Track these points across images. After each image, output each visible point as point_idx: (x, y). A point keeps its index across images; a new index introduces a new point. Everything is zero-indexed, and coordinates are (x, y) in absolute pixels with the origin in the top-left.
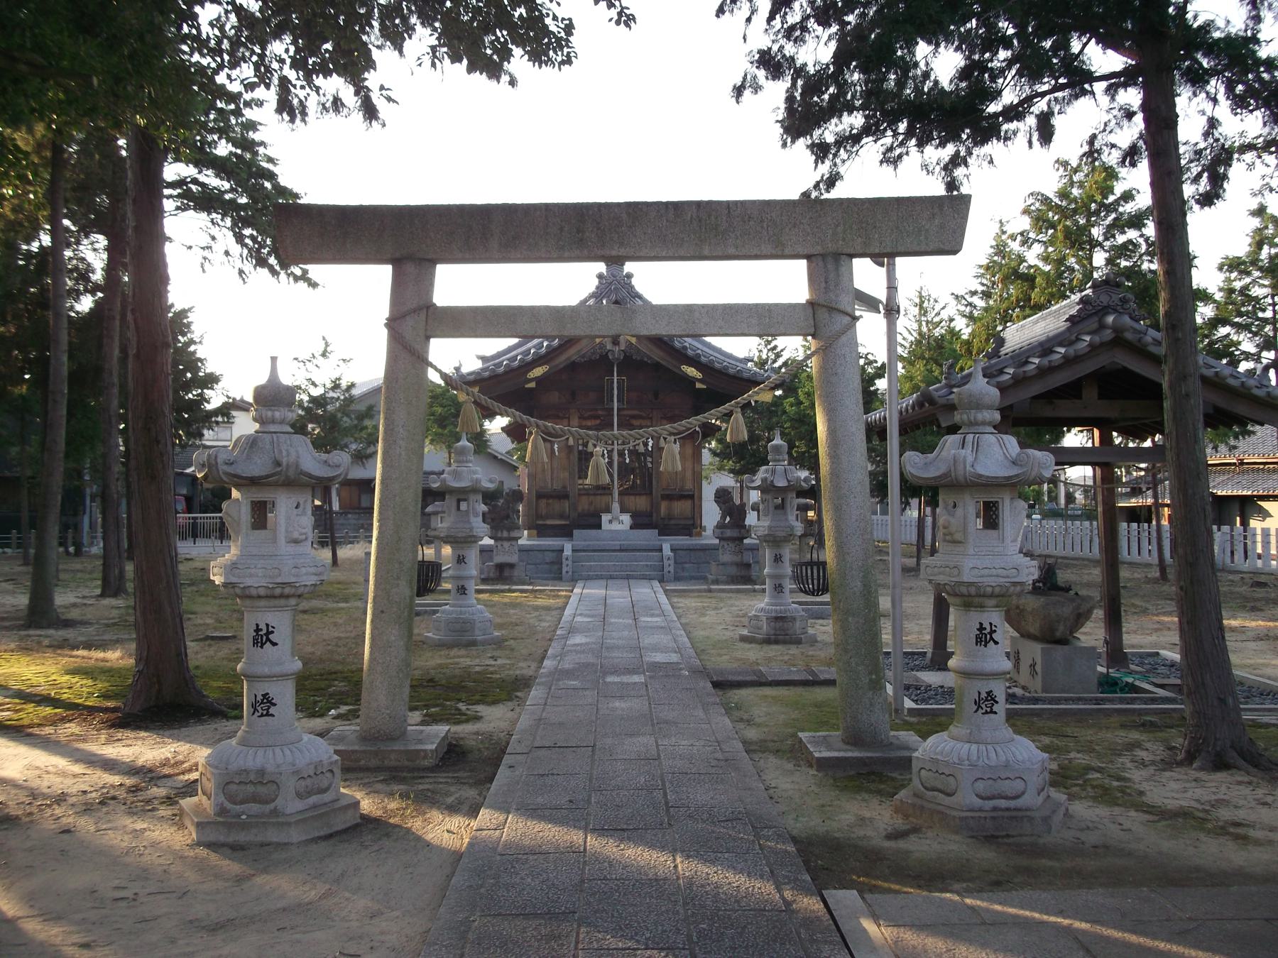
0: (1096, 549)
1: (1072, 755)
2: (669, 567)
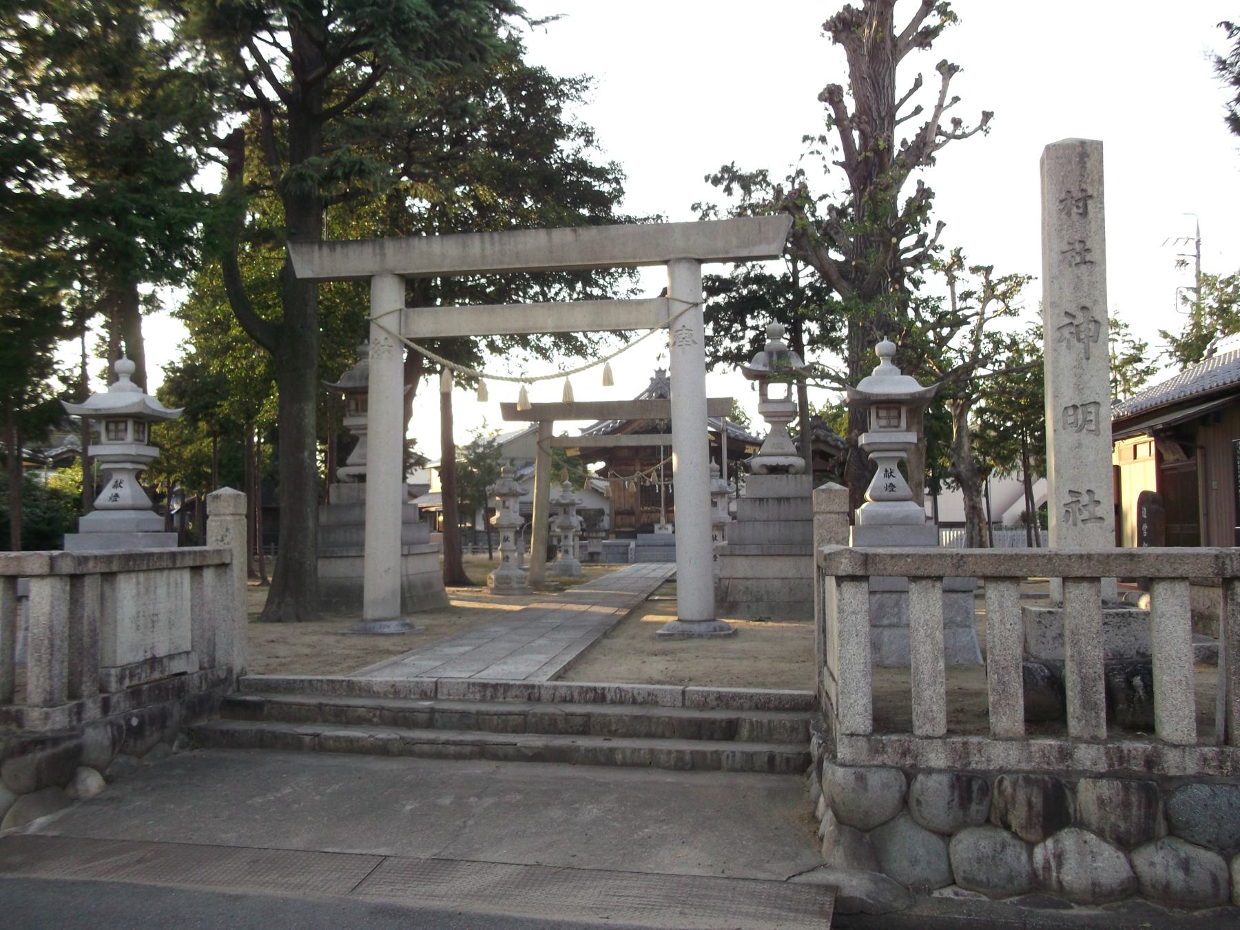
1: (152, 764)
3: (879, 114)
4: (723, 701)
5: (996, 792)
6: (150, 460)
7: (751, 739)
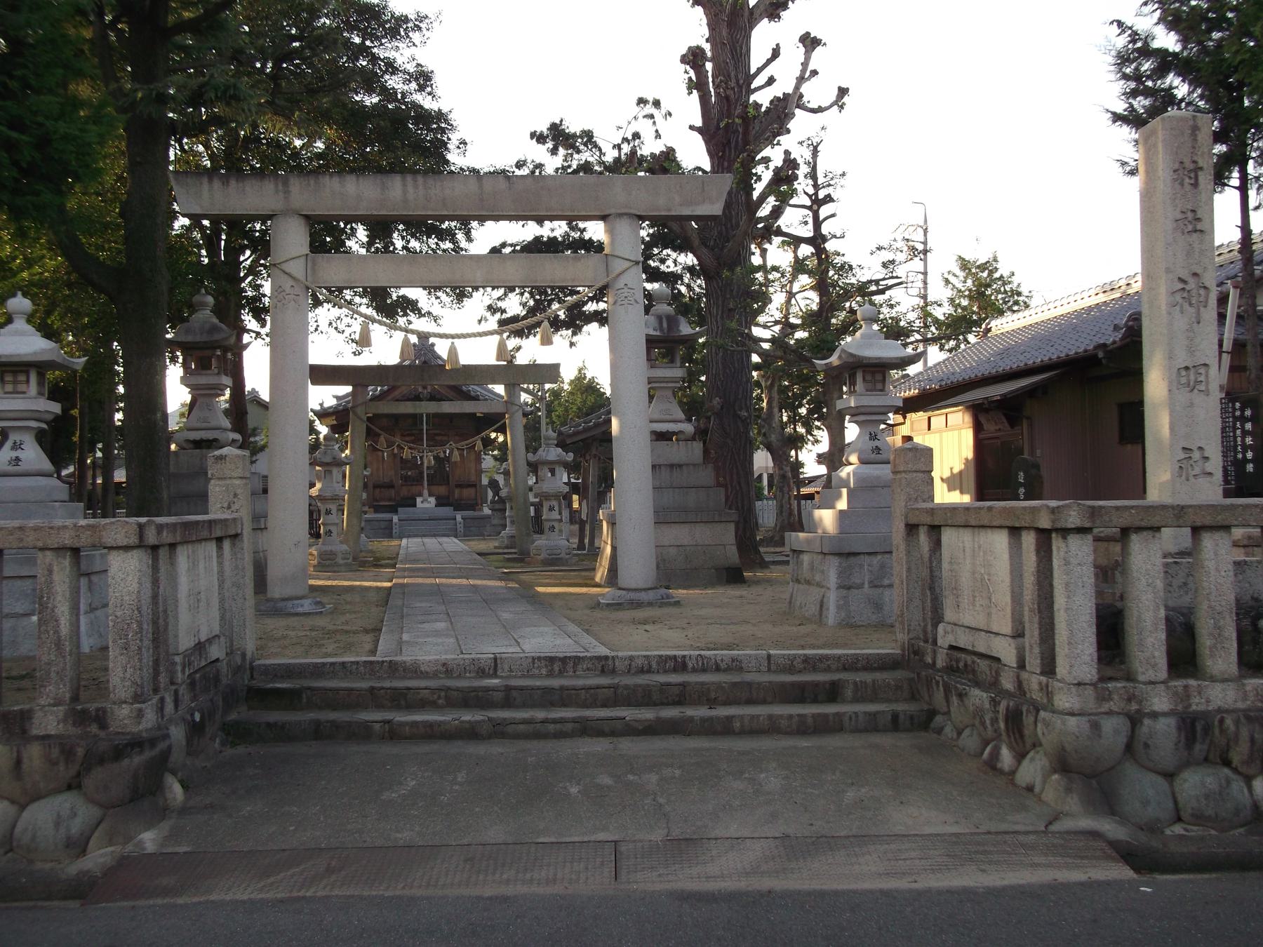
2: (460, 528)
3: (738, 81)
4: (811, 664)
5: (1217, 731)
6: (50, 417)
7: (856, 700)
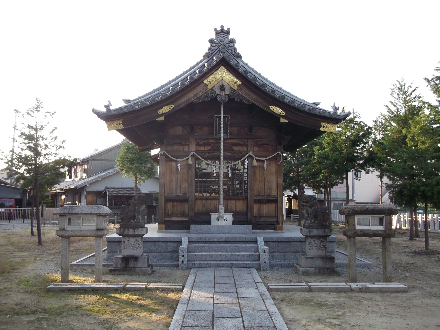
0: (333, 213)
2: (265, 258)
